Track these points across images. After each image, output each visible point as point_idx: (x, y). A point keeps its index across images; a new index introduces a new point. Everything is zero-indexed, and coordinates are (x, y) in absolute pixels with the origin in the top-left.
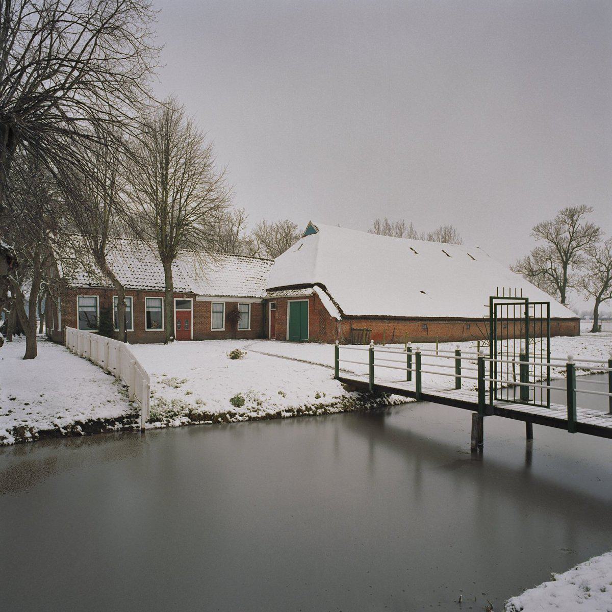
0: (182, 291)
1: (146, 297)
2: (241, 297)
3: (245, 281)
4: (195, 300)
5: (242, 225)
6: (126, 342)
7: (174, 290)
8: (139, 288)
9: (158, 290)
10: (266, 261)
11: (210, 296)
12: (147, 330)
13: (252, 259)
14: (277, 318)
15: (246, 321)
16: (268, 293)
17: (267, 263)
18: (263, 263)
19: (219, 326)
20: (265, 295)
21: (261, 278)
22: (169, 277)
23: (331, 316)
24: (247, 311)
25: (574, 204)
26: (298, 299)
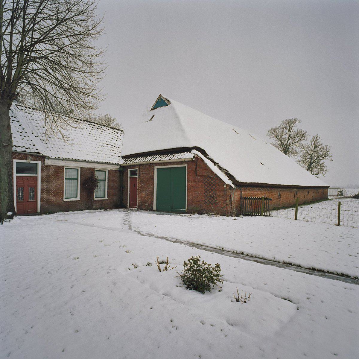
0: (25, 151)
4: (43, 163)
7: (14, 149)
10: (115, 130)
11: (63, 159)
17: (117, 132)
18: (114, 132)
19: (74, 195)
20: (122, 162)
21: (115, 145)
23: (225, 183)
24: (103, 178)
25: (291, 117)
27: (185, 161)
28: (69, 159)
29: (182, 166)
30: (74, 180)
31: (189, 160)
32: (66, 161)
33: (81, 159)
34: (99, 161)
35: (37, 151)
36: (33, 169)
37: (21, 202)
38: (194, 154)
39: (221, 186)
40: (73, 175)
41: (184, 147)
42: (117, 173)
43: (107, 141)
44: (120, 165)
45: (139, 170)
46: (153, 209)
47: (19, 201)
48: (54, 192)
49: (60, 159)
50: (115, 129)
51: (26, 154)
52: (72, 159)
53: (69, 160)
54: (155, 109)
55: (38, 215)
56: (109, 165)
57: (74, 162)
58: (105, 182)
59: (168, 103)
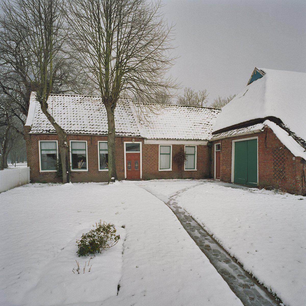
0: (131, 135)
1: (98, 142)
2: (187, 140)
3: (192, 126)
4: (143, 143)
5: (204, 101)
6: (69, 182)
8: (92, 133)
9: (103, 134)
10: (213, 110)
11: (157, 139)
12: (99, 170)
13: (201, 109)
14: (221, 159)
15: (193, 162)
16: (214, 135)
17: (214, 112)
18: (211, 112)
20: (210, 138)
22: (111, 121)
23: (294, 156)
26: (246, 138)
27: (255, 133)
28: (162, 138)
29: (253, 139)
30: (168, 155)
31: (257, 132)
32: (159, 141)
33: (171, 138)
34: (187, 138)
35: (138, 135)
36: (136, 147)
37: (130, 171)
38: (264, 125)
39: (290, 159)
40: (167, 150)
41: (257, 118)
42: (206, 148)
43: (201, 120)
44: (208, 141)
45: (221, 144)
46: (231, 181)
47: (128, 170)
49: (156, 139)
50: (213, 109)
51: (132, 137)
52: (165, 138)
53: (162, 139)
54: (251, 83)
55: (141, 180)
56: (197, 141)
57: (167, 141)
58: (195, 156)
59: (263, 74)
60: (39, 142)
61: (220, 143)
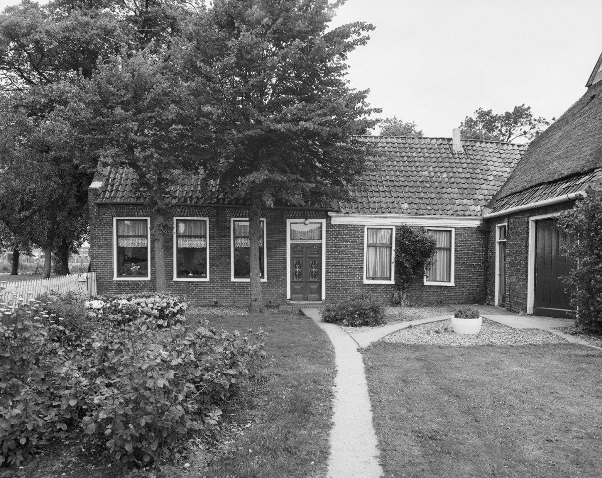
1: (232, 219)
40: (384, 237)
45: (508, 226)
48: (346, 269)
60: (115, 219)
61: (506, 224)
